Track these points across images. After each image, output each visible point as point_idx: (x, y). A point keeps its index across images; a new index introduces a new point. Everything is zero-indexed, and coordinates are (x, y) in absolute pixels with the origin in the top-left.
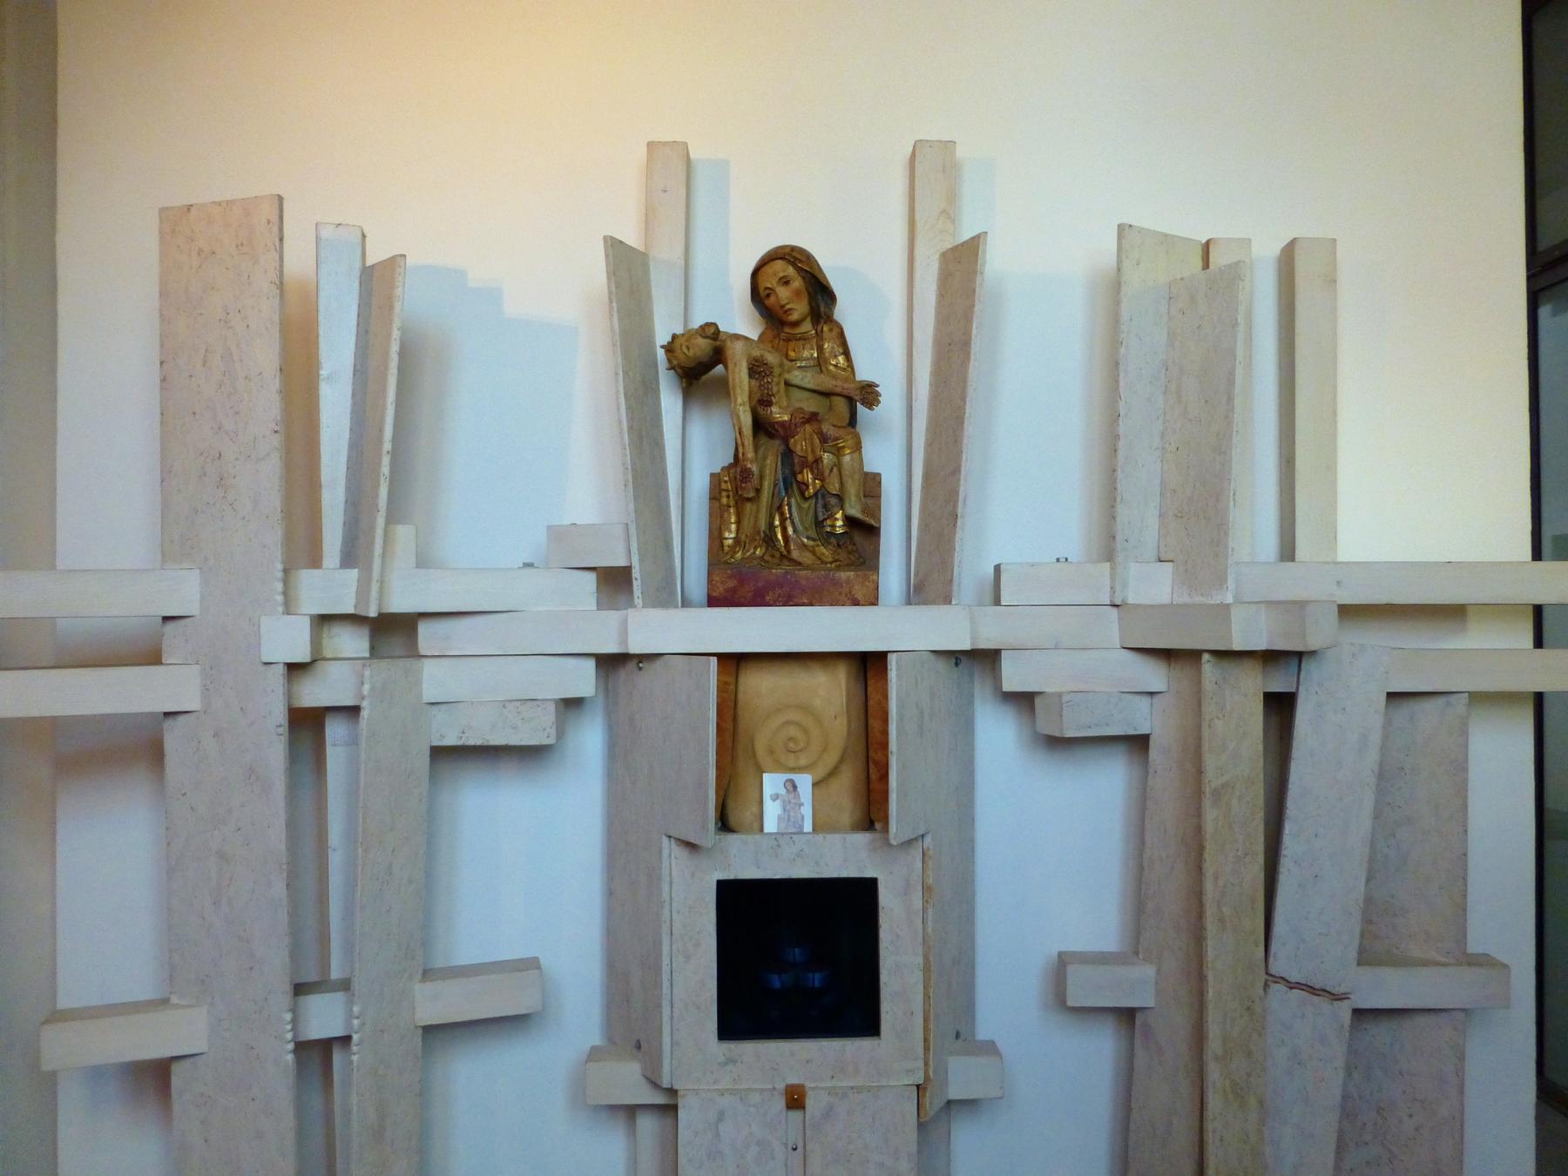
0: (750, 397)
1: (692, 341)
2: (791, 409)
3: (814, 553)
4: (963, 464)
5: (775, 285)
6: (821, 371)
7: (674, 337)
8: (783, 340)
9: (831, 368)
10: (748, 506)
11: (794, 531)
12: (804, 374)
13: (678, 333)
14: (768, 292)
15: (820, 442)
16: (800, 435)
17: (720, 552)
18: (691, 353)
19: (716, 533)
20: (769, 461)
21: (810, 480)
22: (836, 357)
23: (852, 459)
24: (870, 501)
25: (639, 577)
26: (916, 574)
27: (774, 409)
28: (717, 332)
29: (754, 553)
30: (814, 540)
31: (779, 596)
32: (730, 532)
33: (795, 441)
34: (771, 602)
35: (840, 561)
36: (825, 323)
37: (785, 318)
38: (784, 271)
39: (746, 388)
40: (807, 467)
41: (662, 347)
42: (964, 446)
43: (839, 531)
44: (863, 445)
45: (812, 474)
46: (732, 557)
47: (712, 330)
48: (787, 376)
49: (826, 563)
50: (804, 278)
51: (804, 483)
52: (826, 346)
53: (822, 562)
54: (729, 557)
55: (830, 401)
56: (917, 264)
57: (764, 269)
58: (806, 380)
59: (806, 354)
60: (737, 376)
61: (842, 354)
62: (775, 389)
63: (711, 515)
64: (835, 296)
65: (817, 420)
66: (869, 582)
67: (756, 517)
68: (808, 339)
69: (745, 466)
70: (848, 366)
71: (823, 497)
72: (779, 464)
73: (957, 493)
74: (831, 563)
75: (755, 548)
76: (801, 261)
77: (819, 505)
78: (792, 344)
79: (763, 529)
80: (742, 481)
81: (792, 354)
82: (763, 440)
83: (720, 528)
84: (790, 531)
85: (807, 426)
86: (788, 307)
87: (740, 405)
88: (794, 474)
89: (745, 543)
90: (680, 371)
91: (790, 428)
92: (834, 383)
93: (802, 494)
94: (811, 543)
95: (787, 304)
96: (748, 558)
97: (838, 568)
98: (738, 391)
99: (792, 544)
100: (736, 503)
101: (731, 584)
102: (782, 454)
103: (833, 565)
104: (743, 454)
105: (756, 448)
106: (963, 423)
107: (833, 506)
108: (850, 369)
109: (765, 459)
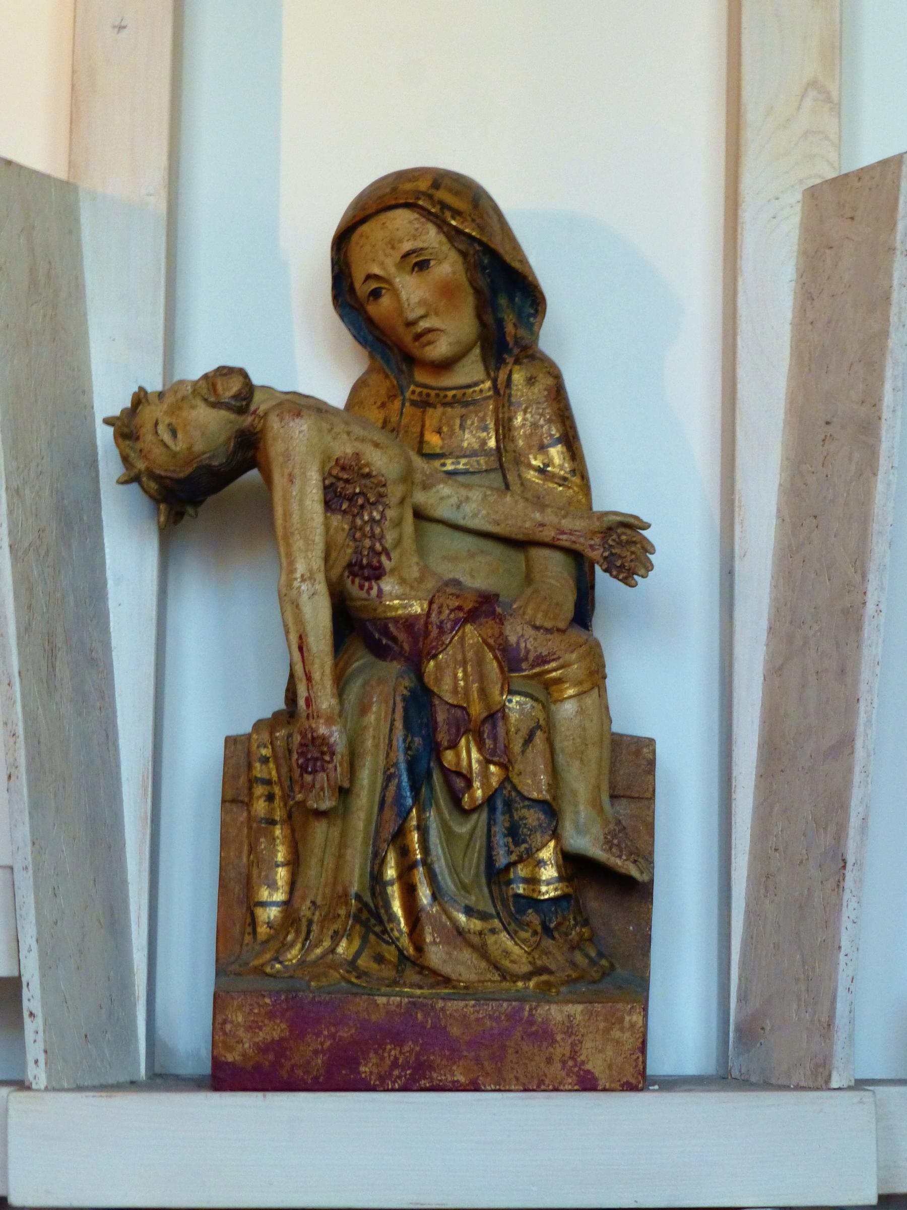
0: (327, 558)
1: (184, 414)
2: (431, 584)
3: (482, 951)
4: (861, 729)
5: (392, 270)
6: (507, 487)
7: (140, 399)
8: (414, 403)
9: (532, 475)
10: (320, 830)
11: (434, 897)
12: (463, 492)
13: (149, 389)
14: (374, 285)
15: (501, 668)
16: (450, 650)
17: (248, 939)
18: (179, 446)
19: (237, 889)
20: (372, 718)
21: (475, 766)
22: (542, 448)
23: (581, 711)
24: (624, 809)
25: (38, 1012)
26: (743, 998)
27: (388, 585)
28: (248, 390)
29: (333, 951)
30: (484, 916)
31: (395, 1064)
32: (272, 886)
33: (438, 667)
34: (374, 1081)
35: (550, 972)
36: (517, 362)
37: (415, 349)
38: (415, 237)
39: (318, 539)
40: (466, 732)
41: (108, 421)
42: (863, 687)
43: (548, 892)
44: (608, 670)
45: (480, 750)
46: (276, 959)
47: (235, 386)
48: (420, 497)
49: (515, 978)
50: (464, 254)
51: (459, 774)
52: (519, 420)
53: (505, 975)
54: (268, 956)
55: (527, 560)
56: (747, 214)
57: (365, 228)
58: (468, 509)
59: (468, 440)
60: (295, 507)
61: (559, 441)
62: (390, 538)
63: (225, 842)
64: (541, 293)
65: (493, 614)
66: (622, 1030)
67: (340, 857)
68: (474, 402)
69: (313, 730)
70: (573, 472)
71: (509, 805)
72: (399, 724)
73: (844, 806)
74: (527, 977)
75: (336, 938)
76: (456, 213)
77: (499, 829)
78: (433, 416)
79: (355, 889)
80: (303, 769)
81: (434, 440)
82: (361, 659)
83: (249, 877)
84: (424, 895)
85: (469, 628)
86: (424, 324)
87: (303, 580)
88: (435, 750)
89: (310, 922)
90: (153, 486)
91: (427, 633)
92: (538, 516)
93: (456, 800)
94: (476, 924)
95: (422, 317)
96: (315, 963)
97: (545, 992)
98: (298, 544)
99: (428, 929)
100: (290, 816)
101: (275, 1031)
102: (404, 699)
103: (531, 984)
104: (308, 701)
105: (341, 682)
106: (859, 629)
107: (533, 831)
108: (576, 480)
109: (364, 710)
